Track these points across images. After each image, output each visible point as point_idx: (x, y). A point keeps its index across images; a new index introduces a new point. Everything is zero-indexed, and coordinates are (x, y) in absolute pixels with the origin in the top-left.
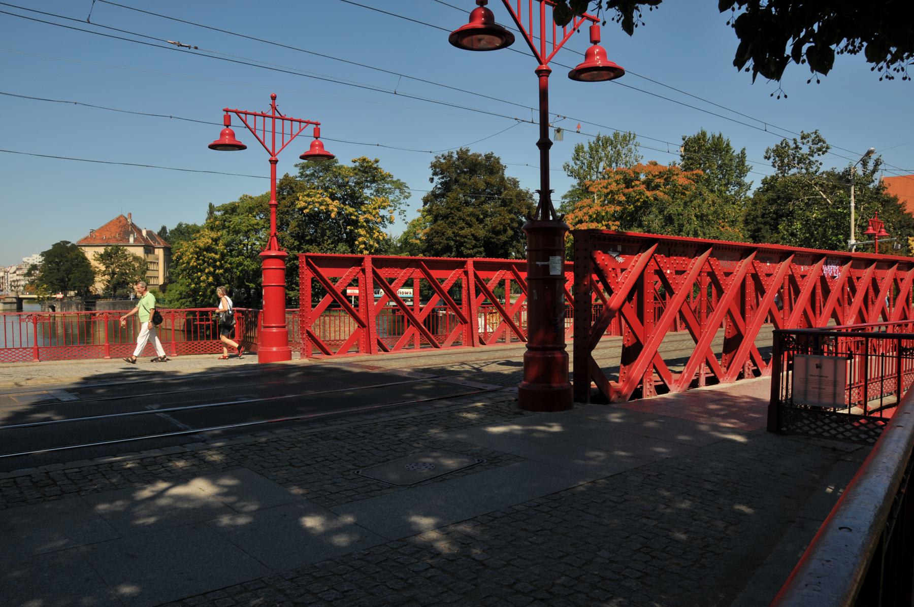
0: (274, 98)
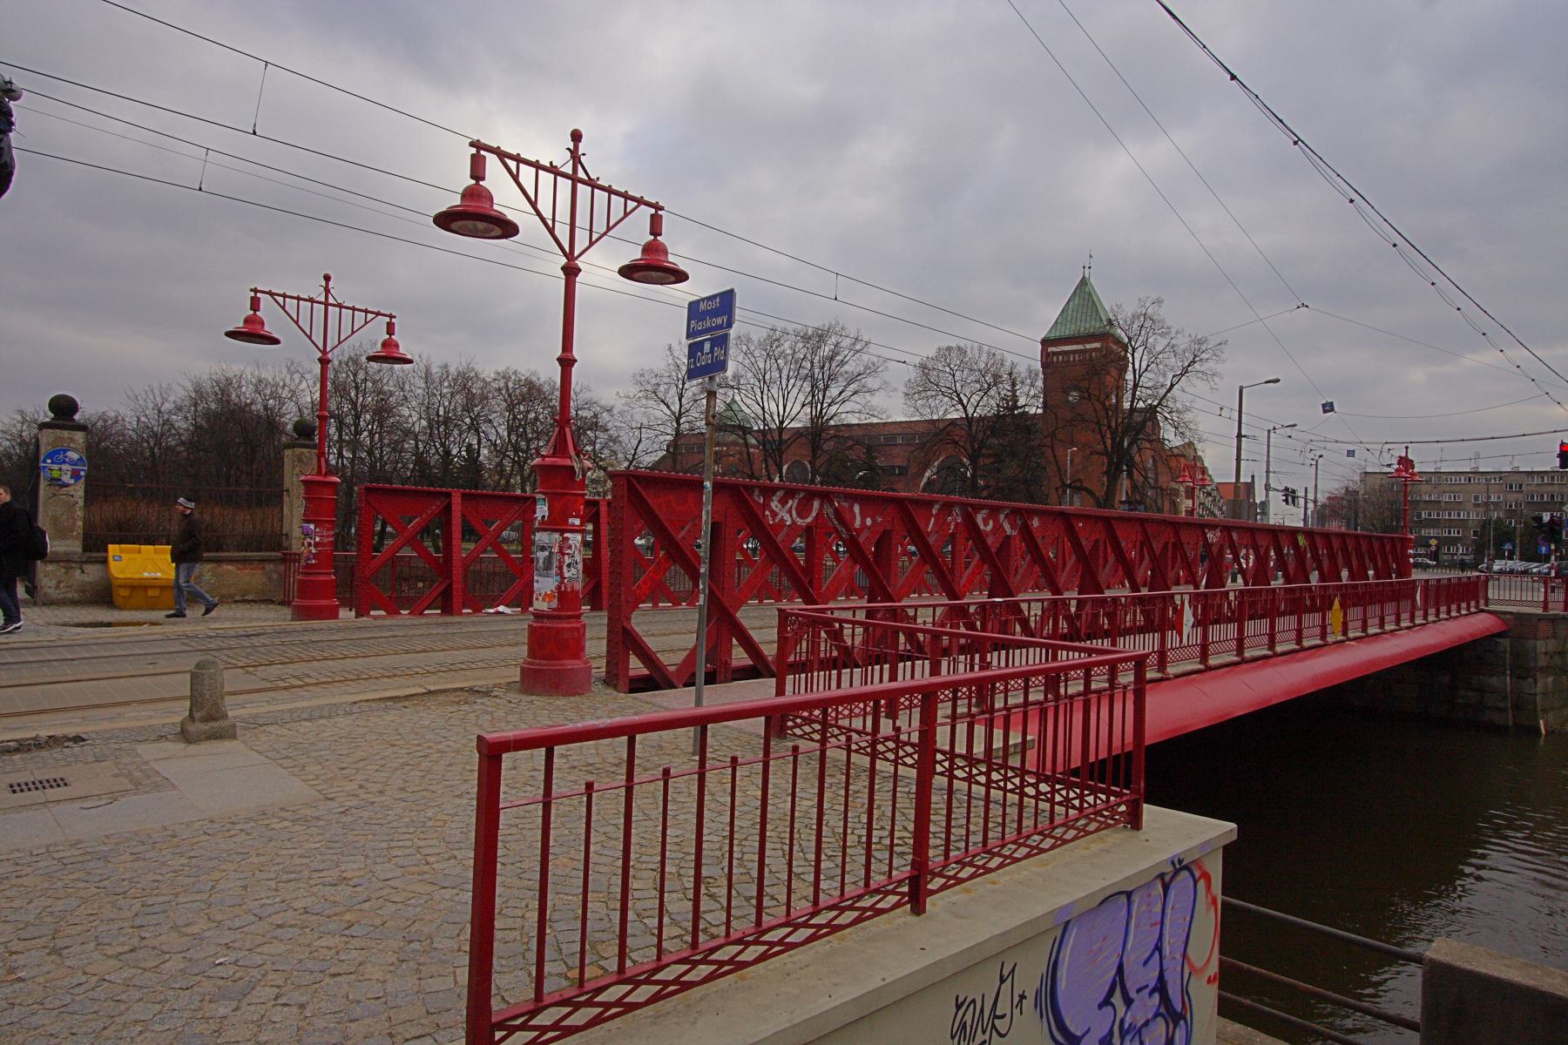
0: (327, 278)
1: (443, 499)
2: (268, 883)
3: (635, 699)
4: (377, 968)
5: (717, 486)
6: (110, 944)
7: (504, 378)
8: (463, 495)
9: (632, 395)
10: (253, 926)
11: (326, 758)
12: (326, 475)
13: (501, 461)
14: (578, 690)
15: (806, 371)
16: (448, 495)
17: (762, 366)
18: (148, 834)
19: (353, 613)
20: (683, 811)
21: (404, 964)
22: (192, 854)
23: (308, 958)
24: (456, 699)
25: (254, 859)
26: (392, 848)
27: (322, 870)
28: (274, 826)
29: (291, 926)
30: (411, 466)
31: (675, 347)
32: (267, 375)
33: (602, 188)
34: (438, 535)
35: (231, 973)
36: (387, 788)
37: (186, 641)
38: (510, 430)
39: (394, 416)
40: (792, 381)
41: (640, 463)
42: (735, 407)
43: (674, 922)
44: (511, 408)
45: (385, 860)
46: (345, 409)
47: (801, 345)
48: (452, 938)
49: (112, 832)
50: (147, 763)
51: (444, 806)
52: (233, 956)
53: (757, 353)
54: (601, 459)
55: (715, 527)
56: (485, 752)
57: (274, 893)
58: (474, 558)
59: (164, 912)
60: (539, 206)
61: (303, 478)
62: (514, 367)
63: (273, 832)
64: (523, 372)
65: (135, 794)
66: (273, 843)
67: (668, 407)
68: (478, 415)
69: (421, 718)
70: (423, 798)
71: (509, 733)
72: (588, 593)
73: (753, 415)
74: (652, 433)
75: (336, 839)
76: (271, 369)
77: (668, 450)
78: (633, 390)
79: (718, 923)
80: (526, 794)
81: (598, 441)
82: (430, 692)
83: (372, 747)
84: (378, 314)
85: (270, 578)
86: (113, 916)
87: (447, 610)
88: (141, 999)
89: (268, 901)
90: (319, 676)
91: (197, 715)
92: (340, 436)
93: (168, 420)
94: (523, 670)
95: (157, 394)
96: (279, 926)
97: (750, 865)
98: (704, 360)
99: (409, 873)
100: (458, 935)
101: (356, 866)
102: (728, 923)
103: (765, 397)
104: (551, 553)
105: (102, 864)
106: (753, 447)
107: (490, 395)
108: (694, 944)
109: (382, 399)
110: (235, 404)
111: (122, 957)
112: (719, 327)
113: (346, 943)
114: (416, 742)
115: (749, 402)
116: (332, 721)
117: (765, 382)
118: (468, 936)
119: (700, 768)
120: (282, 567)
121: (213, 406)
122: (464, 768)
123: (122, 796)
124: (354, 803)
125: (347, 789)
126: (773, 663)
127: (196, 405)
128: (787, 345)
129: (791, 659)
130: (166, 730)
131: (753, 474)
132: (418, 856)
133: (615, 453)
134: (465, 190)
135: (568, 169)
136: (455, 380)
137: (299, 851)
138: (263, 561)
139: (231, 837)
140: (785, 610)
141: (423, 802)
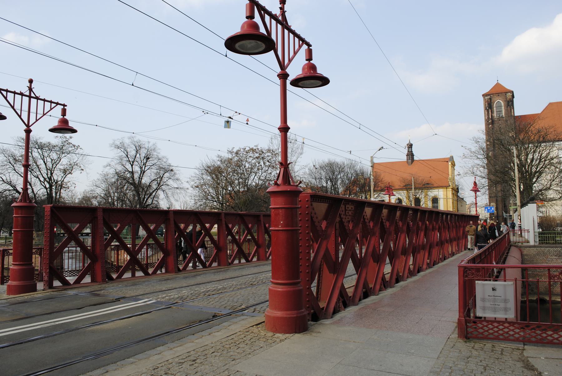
0: (31, 81)
135: (27, 93)
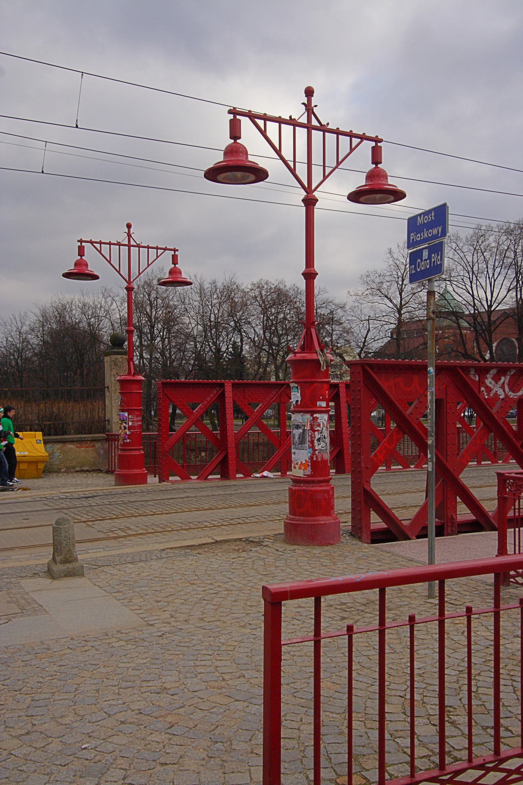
0: (129, 226)
1: (218, 389)
2: (114, 688)
3: (377, 548)
4: (193, 761)
5: (439, 369)
6: (13, 728)
7: (258, 287)
8: (234, 385)
9: (360, 293)
10: (105, 721)
11: (146, 593)
12: (134, 374)
13: (259, 354)
14: (331, 542)
15: (510, 260)
16: (222, 385)
17: (470, 259)
18: (31, 647)
19: (157, 479)
20: (422, 647)
21: (212, 759)
22: (61, 663)
23: (143, 749)
24: (237, 548)
25: (102, 670)
26: (197, 666)
27: (149, 681)
28: (114, 644)
29: (131, 723)
30: (192, 362)
31: (395, 250)
32: (89, 300)
33: (331, 131)
34: (214, 414)
35: (93, 756)
36: (190, 618)
37: (46, 502)
38: (265, 329)
39: (178, 324)
40: (498, 270)
41: (369, 349)
42: (448, 296)
43: (423, 745)
44: (265, 311)
45: (193, 675)
46: (144, 322)
47: (504, 238)
48: (246, 742)
49: (9, 644)
50: (27, 593)
51: (233, 634)
52: (93, 743)
53: (465, 249)
54: (338, 348)
55: (439, 403)
56: (269, 599)
57: (117, 697)
58: (244, 432)
59: (46, 706)
60: (283, 153)
61: (118, 378)
62: (266, 278)
63: (113, 649)
64: (273, 282)
65: (22, 616)
66: (114, 658)
67: (391, 301)
68: (240, 319)
69: (212, 562)
70: (218, 627)
71: (287, 585)
72: (333, 459)
73: (464, 302)
74: (378, 324)
75: (157, 657)
76: (91, 296)
77: (392, 337)
78: (361, 289)
79: (460, 748)
80: (295, 627)
81: (334, 333)
82: (217, 542)
83: (177, 585)
84: (165, 249)
85: (99, 454)
86: (15, 707)
87: (225, 475)
88: (36, 771)
89: (114, 703)
90: (137, 529)
91: (58, 559)
92: (141, 342)
93: (26, 338)
94: (286, 525)
95: (18, 320)
96: (123, 723)
97: (484, 698)
98: (423, 265)
99: (210, 686)
100: (250, 740)
101: (172, 679)
102: (470, 749)
103: (474, 286)
104: (304, 430)
105: (5, 668)
106: (466, 329)
107: (249, 302)
108: (442, 765)
109: (169, 312)
110: (68, 323)
111: (21, 738)
112: (436, 237)
113: (170, 739)
114: (209, 582)
115: (460, 291)
116: (149, 564)
117: (473, 273)
118: (261, 741)
119: (440, 615)
120: (106, 445)
121: (54, 326)
122: (246, 604)
123: (14, 617)
124: (168, 629)
125: (162, 617)
126: (493, 518)
127: (43, 326)
128: (492, 239)
129: (511, 514)
130: (38, 569)
131: (466, 352)
132: (217, 673)
133: (348, 341)
134: (227, 148)
135: (304, 120)
136: (222, 292)
137: (132, 665)
138: (93, 441)
139: (86, 651)
140: (503, 474)
141: (218, 630)
